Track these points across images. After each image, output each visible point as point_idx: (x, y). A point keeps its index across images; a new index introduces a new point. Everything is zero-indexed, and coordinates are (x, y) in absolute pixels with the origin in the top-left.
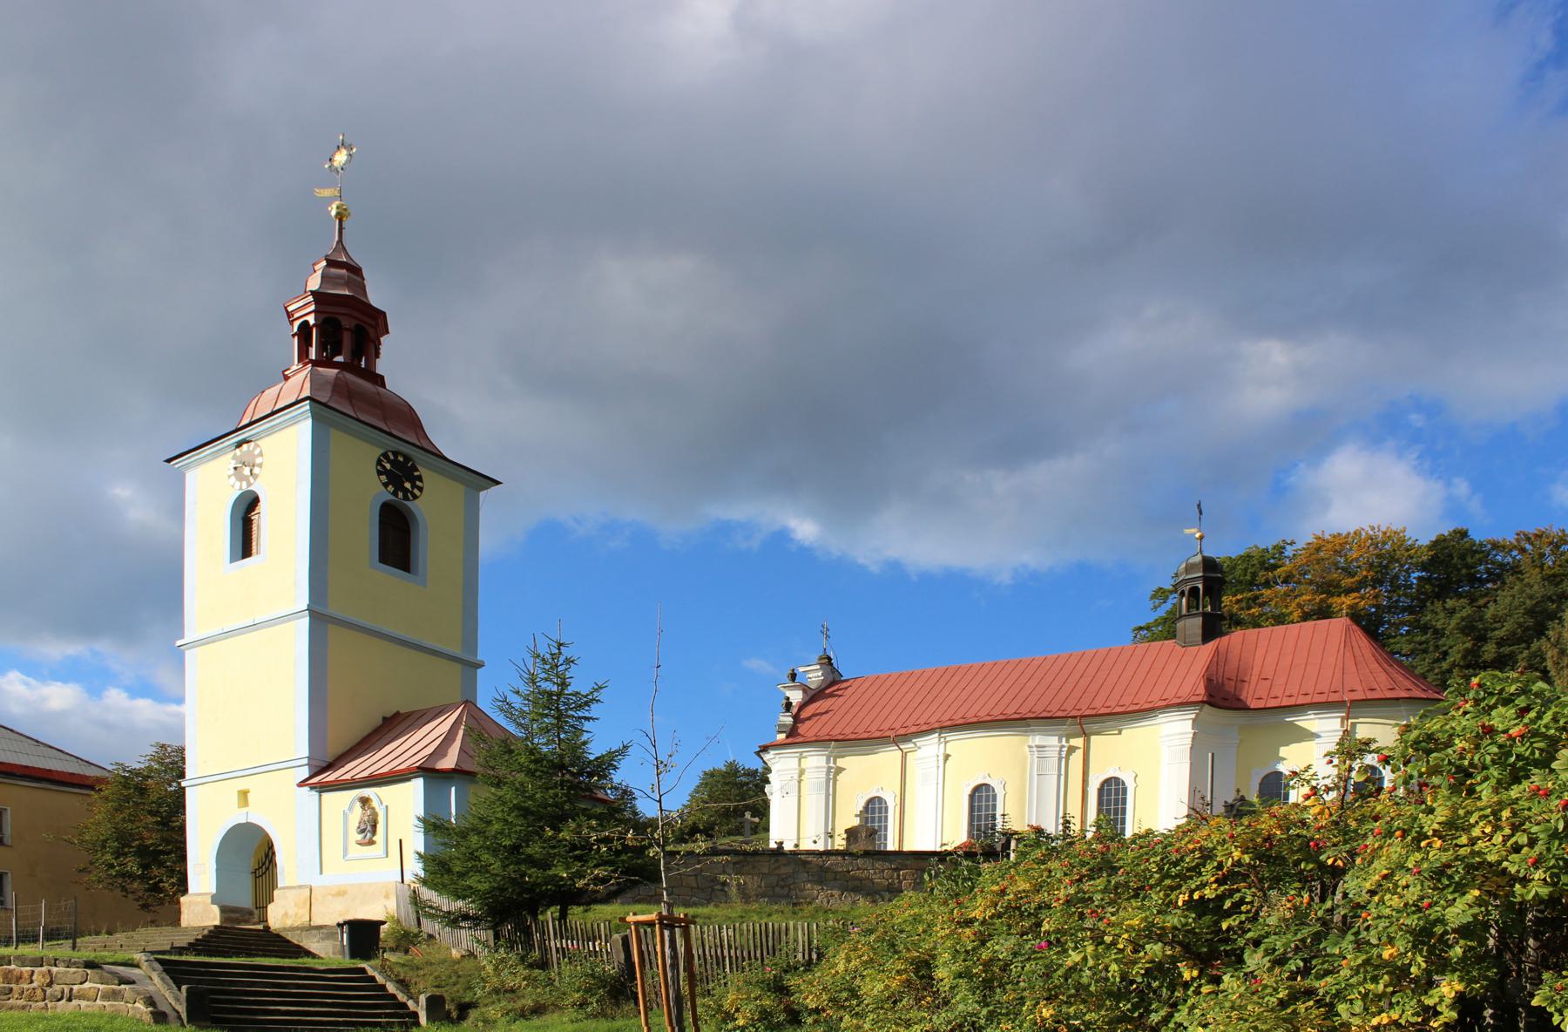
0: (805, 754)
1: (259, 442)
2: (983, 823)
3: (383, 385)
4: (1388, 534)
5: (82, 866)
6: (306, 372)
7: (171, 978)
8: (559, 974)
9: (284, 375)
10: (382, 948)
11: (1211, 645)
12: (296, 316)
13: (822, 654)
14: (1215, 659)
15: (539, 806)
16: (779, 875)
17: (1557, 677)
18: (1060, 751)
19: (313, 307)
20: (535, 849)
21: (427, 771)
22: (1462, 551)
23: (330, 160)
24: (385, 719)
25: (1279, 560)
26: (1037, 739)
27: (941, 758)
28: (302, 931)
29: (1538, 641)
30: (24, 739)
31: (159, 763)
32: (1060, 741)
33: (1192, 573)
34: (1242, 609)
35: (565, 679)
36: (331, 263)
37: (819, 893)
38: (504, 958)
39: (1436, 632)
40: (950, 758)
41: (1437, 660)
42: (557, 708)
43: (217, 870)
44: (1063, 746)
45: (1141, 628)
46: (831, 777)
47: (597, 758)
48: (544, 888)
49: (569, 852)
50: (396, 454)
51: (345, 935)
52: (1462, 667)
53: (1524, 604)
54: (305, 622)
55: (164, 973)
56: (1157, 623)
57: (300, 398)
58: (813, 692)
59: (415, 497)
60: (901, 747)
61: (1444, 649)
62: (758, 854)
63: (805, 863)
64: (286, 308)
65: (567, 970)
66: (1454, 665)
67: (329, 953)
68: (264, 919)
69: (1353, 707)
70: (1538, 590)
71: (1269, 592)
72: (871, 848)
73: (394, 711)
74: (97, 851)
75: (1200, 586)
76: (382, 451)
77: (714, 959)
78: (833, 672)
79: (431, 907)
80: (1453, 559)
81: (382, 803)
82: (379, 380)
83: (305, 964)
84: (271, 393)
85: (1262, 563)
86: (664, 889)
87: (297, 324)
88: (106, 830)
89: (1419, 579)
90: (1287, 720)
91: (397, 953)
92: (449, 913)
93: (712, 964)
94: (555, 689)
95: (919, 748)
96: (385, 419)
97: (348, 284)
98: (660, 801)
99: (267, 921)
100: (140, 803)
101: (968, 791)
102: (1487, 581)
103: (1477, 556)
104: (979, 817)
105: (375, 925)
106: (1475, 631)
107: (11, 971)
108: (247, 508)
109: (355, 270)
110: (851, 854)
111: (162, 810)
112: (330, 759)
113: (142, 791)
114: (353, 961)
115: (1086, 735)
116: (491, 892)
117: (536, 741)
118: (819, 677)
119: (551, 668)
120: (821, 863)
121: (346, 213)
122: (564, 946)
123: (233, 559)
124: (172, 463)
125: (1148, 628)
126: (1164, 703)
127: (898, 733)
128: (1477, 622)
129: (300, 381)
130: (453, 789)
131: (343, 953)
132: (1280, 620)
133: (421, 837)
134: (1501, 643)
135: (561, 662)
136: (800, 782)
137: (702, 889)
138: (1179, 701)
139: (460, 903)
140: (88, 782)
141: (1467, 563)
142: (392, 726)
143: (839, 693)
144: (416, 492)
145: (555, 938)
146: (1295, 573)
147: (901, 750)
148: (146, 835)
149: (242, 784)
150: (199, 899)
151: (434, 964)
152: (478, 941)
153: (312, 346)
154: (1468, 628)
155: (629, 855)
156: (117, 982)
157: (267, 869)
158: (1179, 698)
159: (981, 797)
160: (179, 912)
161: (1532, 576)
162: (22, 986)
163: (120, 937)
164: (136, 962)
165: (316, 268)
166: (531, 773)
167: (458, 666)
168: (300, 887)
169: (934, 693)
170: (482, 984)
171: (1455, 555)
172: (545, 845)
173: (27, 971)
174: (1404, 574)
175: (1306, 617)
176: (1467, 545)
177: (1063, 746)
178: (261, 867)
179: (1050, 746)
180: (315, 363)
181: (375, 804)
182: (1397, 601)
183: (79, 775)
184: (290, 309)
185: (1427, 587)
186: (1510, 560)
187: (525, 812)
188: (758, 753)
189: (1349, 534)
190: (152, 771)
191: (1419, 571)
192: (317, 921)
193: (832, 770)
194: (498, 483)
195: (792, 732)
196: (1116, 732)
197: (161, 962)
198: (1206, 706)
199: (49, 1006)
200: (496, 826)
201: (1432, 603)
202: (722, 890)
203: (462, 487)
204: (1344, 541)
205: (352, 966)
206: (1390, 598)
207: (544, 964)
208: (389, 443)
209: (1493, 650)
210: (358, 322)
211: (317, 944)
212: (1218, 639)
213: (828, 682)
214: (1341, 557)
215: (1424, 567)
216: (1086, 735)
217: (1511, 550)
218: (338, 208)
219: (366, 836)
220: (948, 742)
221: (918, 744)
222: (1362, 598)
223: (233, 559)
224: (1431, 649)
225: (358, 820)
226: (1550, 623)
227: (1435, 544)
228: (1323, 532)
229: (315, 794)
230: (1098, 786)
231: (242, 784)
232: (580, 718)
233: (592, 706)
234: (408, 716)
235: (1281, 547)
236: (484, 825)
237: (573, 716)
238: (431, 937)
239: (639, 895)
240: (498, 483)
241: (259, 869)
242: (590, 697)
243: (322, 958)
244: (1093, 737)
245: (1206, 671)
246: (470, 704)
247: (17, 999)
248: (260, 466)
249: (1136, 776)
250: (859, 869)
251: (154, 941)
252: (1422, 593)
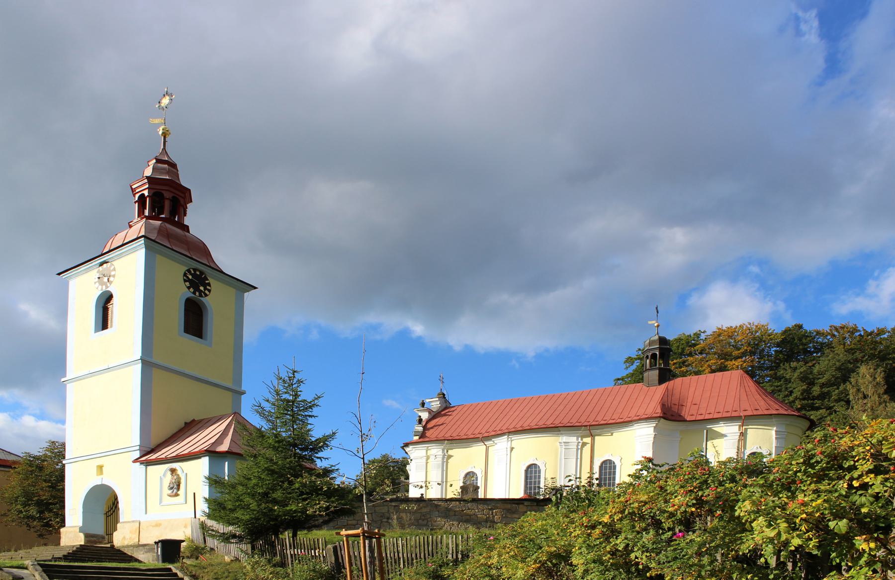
0: (430, 448)
1: (113, 263)
2: (533, 486)
4: (758, 327)
5: (3, 512)
6: (141, 223)
7: (47, 575)
8: (293, 570)
9: (132, 188)
10: (182, 557)
11: (664, 386)
12: (137, 191)
14: (666, 393)
15: (281, 468)
16: (421, 513)
17: (855, 405)
18: (578, 445)
19: (147, 186)
20: (278, 495)
21: (211, 453)
22: (800, 336)
23: (159, 102)
24: (186, 423)
25: (697, 341)
26: (565, 439)
27: (509, 450)
28: (134, 547)
29: (844, 385)
31: (51, 452)
32: (577, 439)
33: (653, 346)
34: (677, 368)
35: (297, 392)
36: (159, 161)
37: (445, 523)
38: (258, 561)
39: (786, 380)
40: (514, 450)
41: (787, 396)
42: (292, 410)
43: (83, 512)
44: (579, 442)
45: (619, 379)
46: (445, 460)
47: (317, 440)
48: (283, 518)
49: (299, 497)
50: (195, 270)
51: (159, 549)
52: (801, 399)
53: (835, 364)
54: (139, 367)
55: (43, 572)
56: (627, 376)
57: (139, 236)
58: (435, 413)
59: (206, 295)
60: (486, 443)
61: (790, 389)
62: (410, 501)
63: (437, 506)
64: (131, 186)
65: (298, 567)
66: (796, 398)
67: (150, 559)
68: (111, 541)
69: (746, 419)
70: (843, 357)
71: (692, 358)
72: (475, 497)
73: (192, 419)
74: (12, 503)
75: (658, 353)
76: (187, 269)
77: (393, 560)
78: (446, 402)
79: (213, 530)
80: (795, 340)
81: (183, 472)
82: (186, 228)
83: (134, 566)
84: (121, 235)
85: (687, 343)
86: (366, 514)
87: (137, 196)
88: (18, 491)
89: (776, 351)
90: (708, 427)
91: (191, 559)
92: (224, 533)
93: (391, 562)
94: (291, 398)
95: (496, 444)
96: (189, 250)
97: (168, 173)
98: (363, 458)
99: (113, 542)
100: (39, 476)
101: (525, 468)
102: (814, 352)
103: (808, 339)
104: (531, 483)
105: (179, 542)
106: (808, 380)
108: (105, 302)
109: (173, 165)
110: (464, 501)
111: (52, 479)
112: (152, 447)
113: (41, 468)
114: (163, 564)
115: (592, 436)
116: (250, 520)
117: (279, 430)
119: (289, 386)
120: (446, 506)
121: (168, 133)
122: (296, 553)
123: (96, 331)
124: (61, 275)
125: (622, 379)
126: (638, 418)
127: (484, 436)
128: (809, 374)
129: (139, 227)
130: (227, 463)
131: (158, 560)
132: (698, 373)
133: (207, 488)
134: (823, 386)
135: (295, 381)
136: (427, 463)
137: (375, 521)
138: (647, 416)
139: (231, 528)
140: (8, 464)
141: (803, 343)
142: (190, 427)
143: (450, 413)
144: (207, 292)
145: (290, 548)
146: (706, 348)
147: (485, 445)
148: (41, 493)
149: (99, 462)
151: (214, 565)
152: (242, 551)
153: (146, 209)
154: (804, 378)
155: (336, 498)
157: (114, 511)
158: (646, 415)
159: (532, 472)
160: (59, 538)
161: (840, 349)
163: (22, 553)
164: (25, 566)
165: (150, 163)
166: (275, 449)
167: (230, 393)
168: (133, 521)
169: (505, 413)
170: (244, 577)
171: (796, 338)
172: (284, 492)
174: (767, 348)
175: (713, 371)
176: (803, 333)
177: (579, 442)
178: (110, 511)
179: (571, 443)
180: (148, 218)
181: (179, 472)
182: (763, 364)
184: (134, 187)
185: (780, 355)
186: (826, 341)
187: (272, 472)
188: (403, 448)
189: (737, 327)
190: (47, 457)
191: (775, 347)
192: (142, 542)
194: (255, 288)
195: (422, 435)
196: (610, 434)
197: (41, 565)
198: (662, 419)
200: (254, 481)
201: (784, 364)
202: (387, 522)
203: (234, 290)
204: (734, 330)
205: (163, 567)
206: (760, 362)
207: (283, 564)
208: (193, 264)
209: (819, 390)
210: (173, 195)
211: (143, 555)
212: (667, 383)
213: (443, 408)
214: (732, 339)
215: (778, 345)
216: (592, 436)
217: (827, 336)
218: (163, 129)
220: (513, 440)
221: (495, 442)
222: (744, 362)
223: (96, 331)
224: (783, 389)
225: (169, 482)
226: (852, 374)
227: (785, 332)
228: (722, 326)
229: (143, 467)
230: (599, 465)
231: (99, 462)
232: (306, 416)
233: (314, 409)
234: (199, 422)
235: (698, 334)
236: (246, 481)
237: (302, 415)
238: (212, 549)
239: (337, 525)
240: (255, 288)
241: (108, 512)
242: (313, 403)
243: (145, 563)
244: (596, 437)
245: (661, 400)
246: (237, 414)
248: (114, 276)
249: (622, 458)
250: (469, 509)
251: (43, 554)
252: (777, 359)
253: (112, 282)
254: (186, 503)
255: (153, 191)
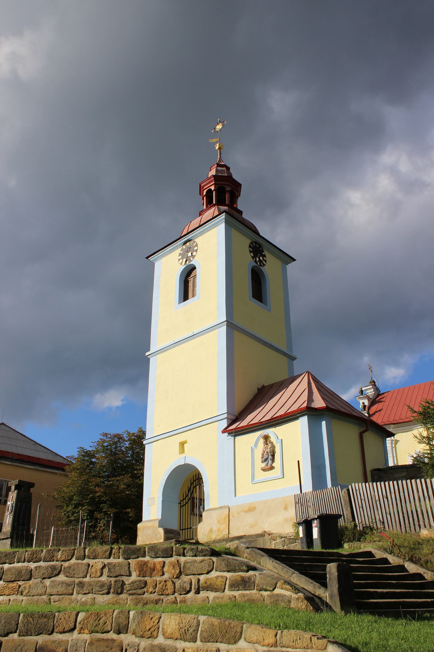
1: (195, 240)
3: (242, 215)
12: (205, 188)
13: (371, 380)
19: (213, 182)
30: (30, 441)
36: (219, 165)
54: (224, 329)
81: (278, 438)
107: (146, 563)
118: (372, 392)
123: (180, 303)
130: (324, 423)
150: (150, 524)
156: (245, 568)
162: (155, 578)
168: (221, 508)
173: (159, 563)
178: (185, 498)
181: (273, 439)
183: (52, 461)
192: (234, 533)
193: (394, 442)
199: (178, 600)
213: (376, 395)
219: (268, 463)
229: (231, 438)
234: (272, 386)
240: (294, 260)
241: (183, 500)
247: (151, 593)
248: (196, 251)
253: (195, 256)
254: (283, 477)
255: (218, 186)
